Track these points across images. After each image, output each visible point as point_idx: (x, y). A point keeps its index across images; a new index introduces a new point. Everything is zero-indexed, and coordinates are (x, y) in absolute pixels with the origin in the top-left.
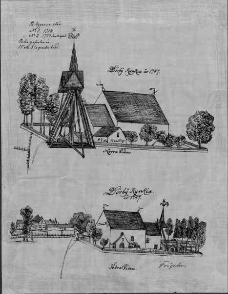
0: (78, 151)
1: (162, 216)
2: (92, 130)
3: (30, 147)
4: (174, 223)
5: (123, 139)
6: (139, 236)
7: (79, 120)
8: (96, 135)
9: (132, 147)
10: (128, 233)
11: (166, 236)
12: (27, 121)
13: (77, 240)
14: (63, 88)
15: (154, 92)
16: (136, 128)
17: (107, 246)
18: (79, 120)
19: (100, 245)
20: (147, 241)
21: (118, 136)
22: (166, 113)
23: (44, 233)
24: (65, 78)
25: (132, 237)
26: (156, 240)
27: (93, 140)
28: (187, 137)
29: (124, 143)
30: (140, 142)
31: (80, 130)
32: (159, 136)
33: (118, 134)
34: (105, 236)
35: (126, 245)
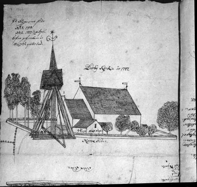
0: (59, 142)
3: (15, 140)
5: (99, 130)
7: (59, 113)
8: (76, 127)
9: (107, 135)
12: (10, 112)
14: (44, 86)
15: (127, 86)
16: (112, 119)
18: (59, 113)
22: (39, 84)
24: (45, 75)
27: (72, 130)
28: (158, 127)
29: (101, 133)
32: (134, 127)
33: (96, 125)
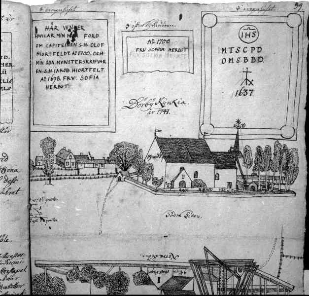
0: (214, 256)
1: (237, 143)
2: (196, 285)
3: (281, 260)
4: (254, 151)
6: (206, 171)
8: (189, 278)
10: (190, 168)
11: (244, 169)
13: (120, 180)
17: (162, 186)
19: (152, 185)
20: (217, 177)
21: (159, 278)
23: (74, 172)
25: (196, 174)
26: (228, 176)
27: (194, 273)
28: (65, 280)
29: (151, 269)
30: (130, 272)
31: (211, 284)
33: (159, 282)
34: (158, 173)
35: (188, 184)
